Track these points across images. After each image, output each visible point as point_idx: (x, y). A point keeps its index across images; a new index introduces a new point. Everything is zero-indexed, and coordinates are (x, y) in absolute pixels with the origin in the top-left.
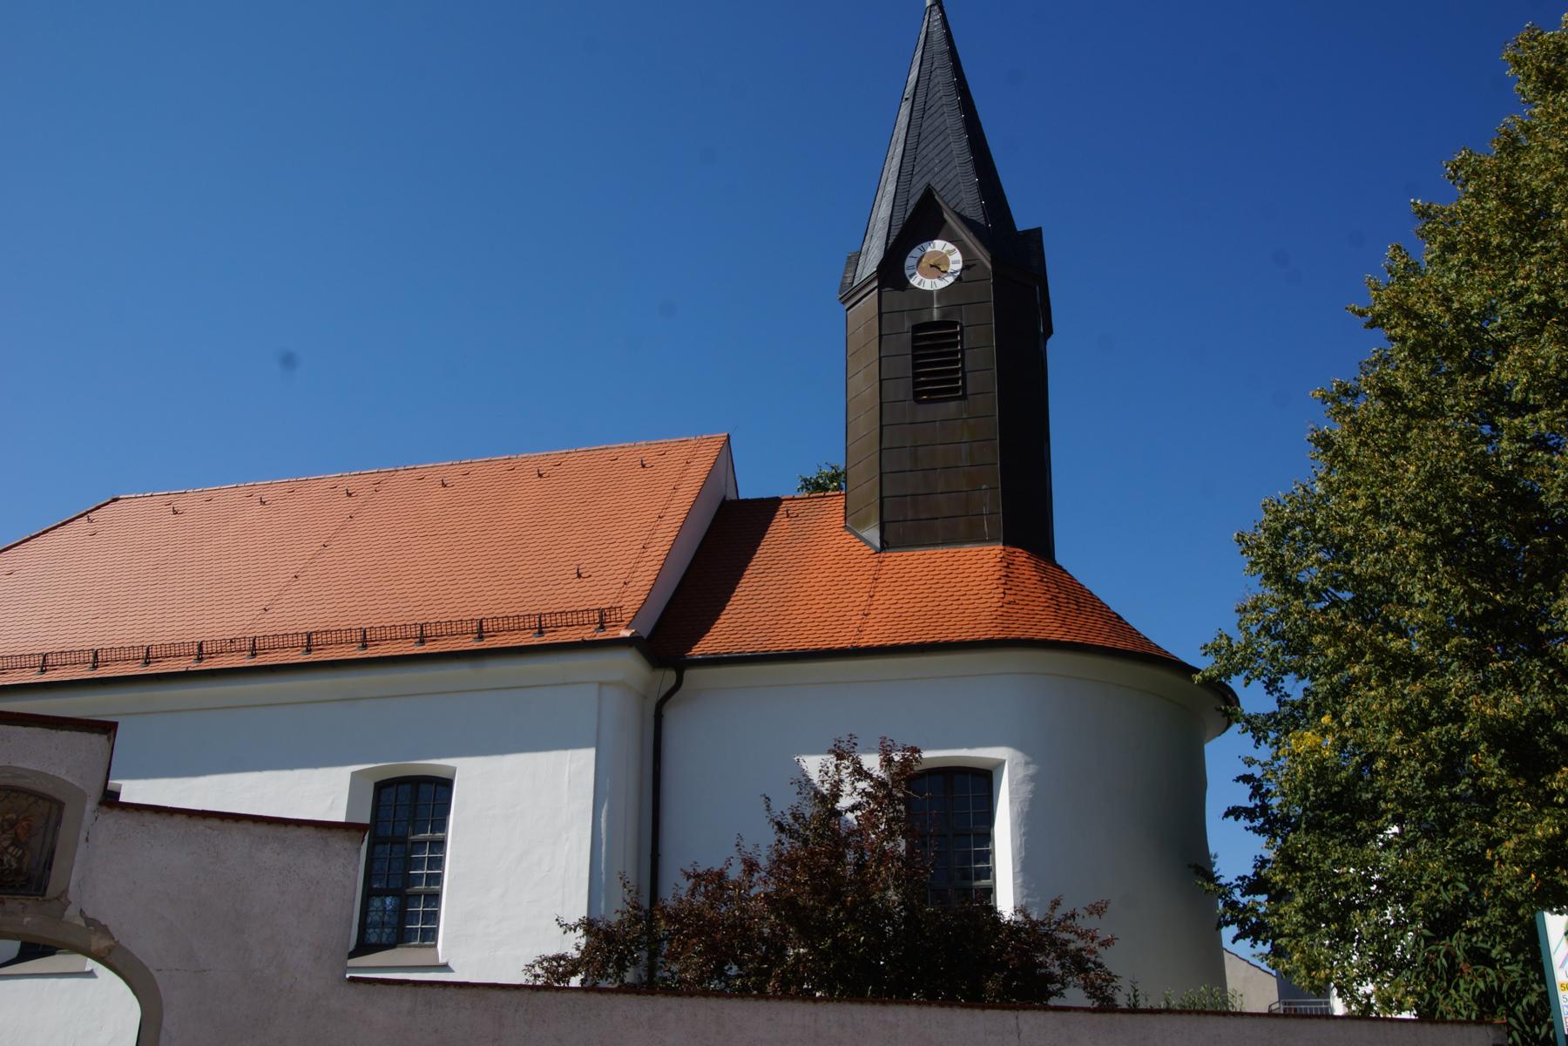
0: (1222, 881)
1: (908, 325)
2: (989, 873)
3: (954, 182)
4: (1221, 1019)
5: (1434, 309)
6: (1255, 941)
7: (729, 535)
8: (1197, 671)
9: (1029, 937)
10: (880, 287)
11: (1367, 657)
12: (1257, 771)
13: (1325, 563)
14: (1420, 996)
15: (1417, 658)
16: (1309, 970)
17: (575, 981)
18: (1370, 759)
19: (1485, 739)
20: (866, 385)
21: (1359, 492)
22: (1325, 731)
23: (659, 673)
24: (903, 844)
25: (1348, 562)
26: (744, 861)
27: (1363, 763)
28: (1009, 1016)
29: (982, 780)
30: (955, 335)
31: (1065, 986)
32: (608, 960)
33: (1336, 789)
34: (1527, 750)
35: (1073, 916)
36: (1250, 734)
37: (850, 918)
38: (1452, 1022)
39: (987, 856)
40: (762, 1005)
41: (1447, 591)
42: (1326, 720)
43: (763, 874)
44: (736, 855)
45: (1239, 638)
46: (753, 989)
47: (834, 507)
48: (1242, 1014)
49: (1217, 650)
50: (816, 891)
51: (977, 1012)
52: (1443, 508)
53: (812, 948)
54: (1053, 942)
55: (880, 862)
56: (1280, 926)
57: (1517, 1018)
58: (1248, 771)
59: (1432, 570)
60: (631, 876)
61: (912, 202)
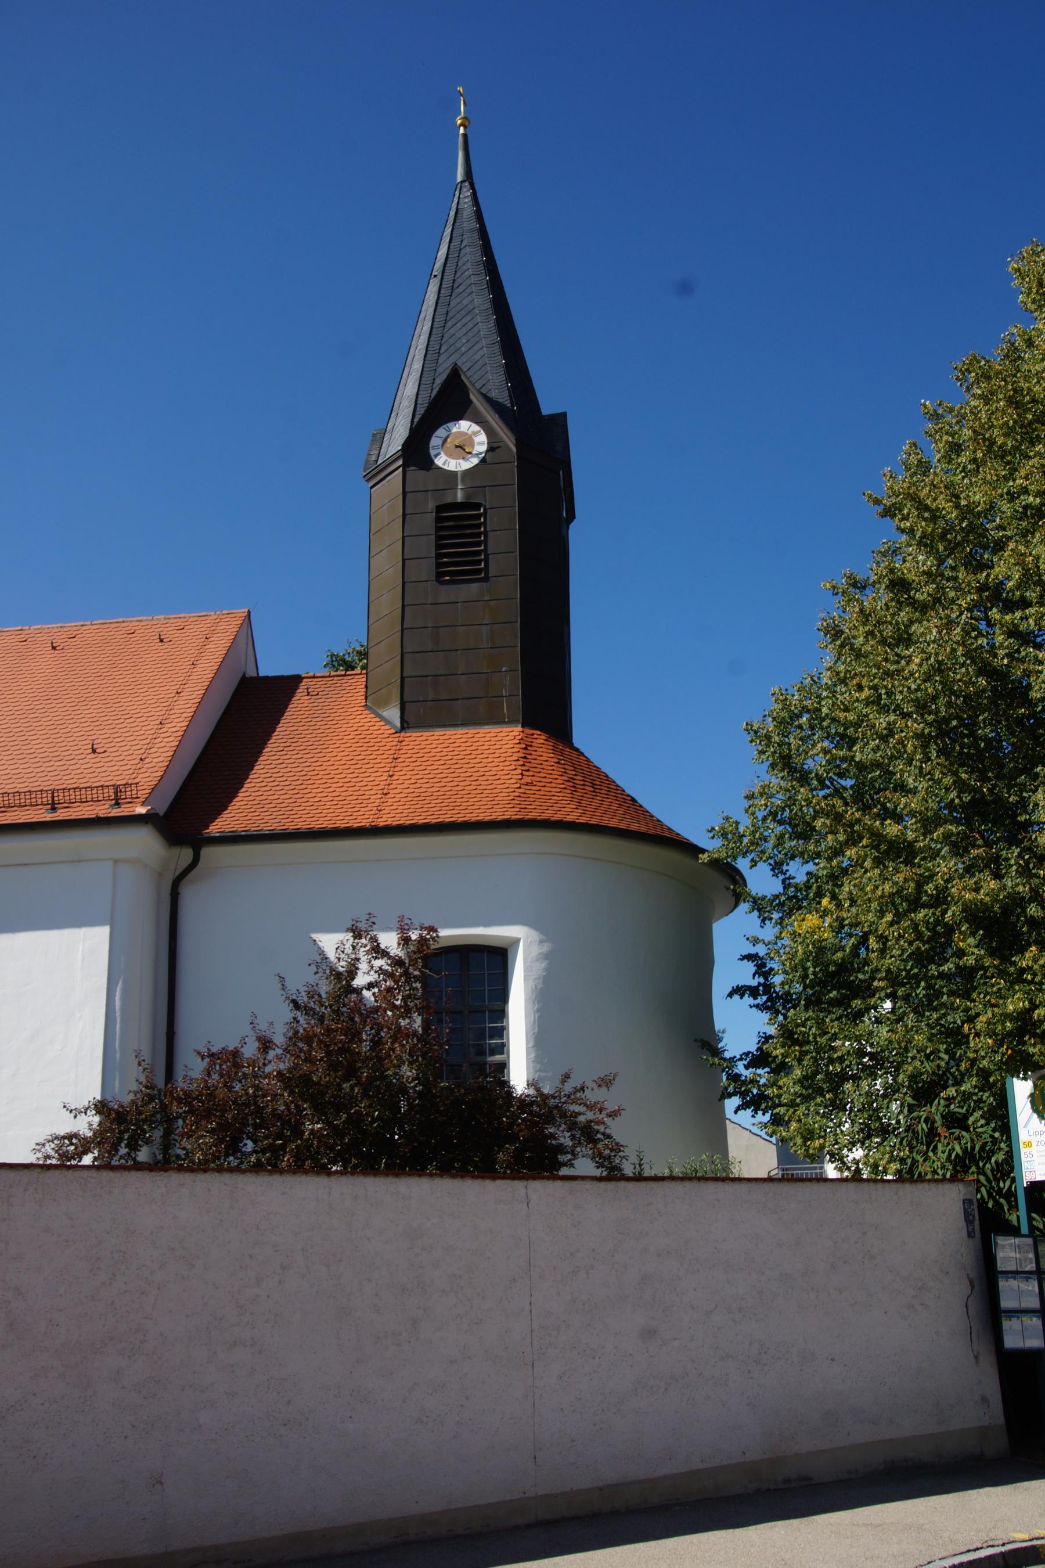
0: (727, 1055)
1: (431, 505)
2: (502, 1048)
4: (720, 1184)
5: (943, 503)
6: (756, 1111)
7: (249, 711)
8: (703, 851)
9: (542, 1109)
10: (405, 466)
11: (864, 842)
12: (761, 950)
13: (829, 751)
14: (902, 1161)
15: (911, 844)
16: (805, 1140)
17: (87, 1160)
18: (864, 940)
19: (967, 921)
21: (864, 682)
22: (825, 913)
23: (176, 850)
24: (418, 1021)
25: (850, 750)
26: (259, 1039)
27: (859, 943)
28: (519, 1186)
29: (496, 959)
30: (478, 516)
31: (575, 1155)
32: (120, 1140)
33: (832, 968)
34: (1002, 929)
35: (582, 1089)
36: (756, 913)
37: (365, 1094)
38: (929, 1181)
39: (501, 1032)
40: (276, 1178)
41: (940, 781)
42: (825, 902)
43: (280, 1051)
44: (251, 1033)
45: (745, 823)
46: (268, 1164)
47: (357, 683)
48: (740, 1180)
49: (724, 835)
50: (333, 1066)
51: (488, 1183)
52: (942, 701)
53: (329, 1124)
54: (563, 1115)
55: (395, 1039)
56: (779, 1096)
57: (985, 1175)
58: (753, 950)
59: (927, 759)
60: (146, 1055)
61: (439, 381)
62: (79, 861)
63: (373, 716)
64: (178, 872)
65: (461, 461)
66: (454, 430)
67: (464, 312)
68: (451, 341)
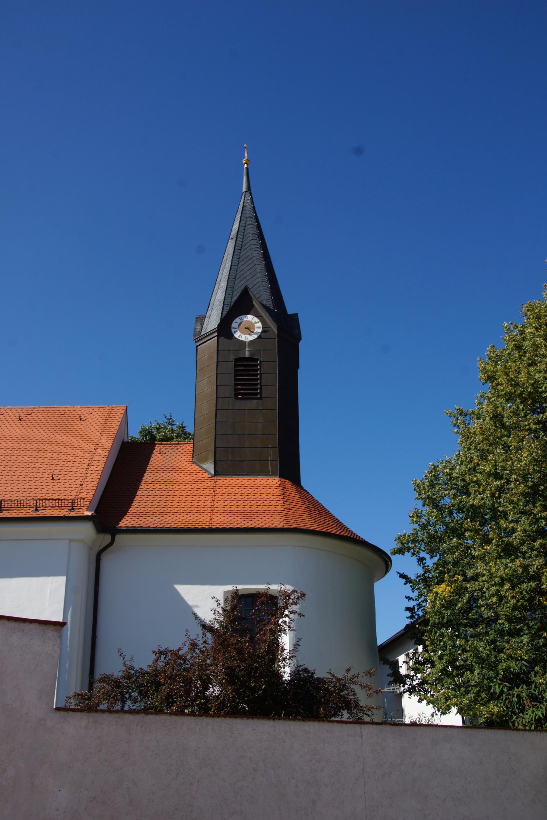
1: (232, 358)
3: (257, 286)
20: (208, 386)
23: (102, 536)
30: (257, 365)
62: (50, 539)
63: (197, 467)
64: (101, 548)
65: (248, 336)
66: (245, 319)
67: (248, 259)
68: (242, 273)
